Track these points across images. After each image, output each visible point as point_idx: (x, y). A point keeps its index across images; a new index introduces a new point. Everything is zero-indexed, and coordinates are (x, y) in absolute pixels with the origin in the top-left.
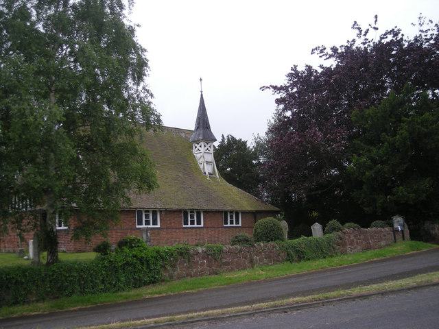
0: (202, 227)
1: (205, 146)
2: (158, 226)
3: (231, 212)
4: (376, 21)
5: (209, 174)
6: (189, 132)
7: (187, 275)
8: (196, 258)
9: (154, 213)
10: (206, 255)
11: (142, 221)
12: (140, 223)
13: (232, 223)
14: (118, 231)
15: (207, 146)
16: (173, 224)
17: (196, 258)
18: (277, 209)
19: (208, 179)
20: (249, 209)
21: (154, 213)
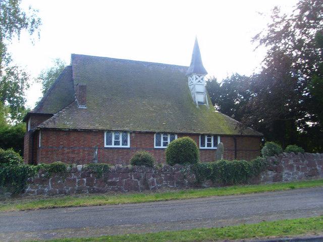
0: (129, 148)
1: (197, 79)
2: (128, 146)
3: (209, 135)
4: (259, 13)
5: (199, 102)
6: (186, 68)
7: (61, 192)
8: (73, 176)
9: (216, 137)
10: (85, 173)
11: (204, 143)
12: (203, 145)
13: (209, 145)
14: (85, 149)
15: (199, 79)
16: (143, 145)
17: (73, 176)
18: (261, 134)
19: (197, 107)
20: (228, 133)
21: (216, 137)
